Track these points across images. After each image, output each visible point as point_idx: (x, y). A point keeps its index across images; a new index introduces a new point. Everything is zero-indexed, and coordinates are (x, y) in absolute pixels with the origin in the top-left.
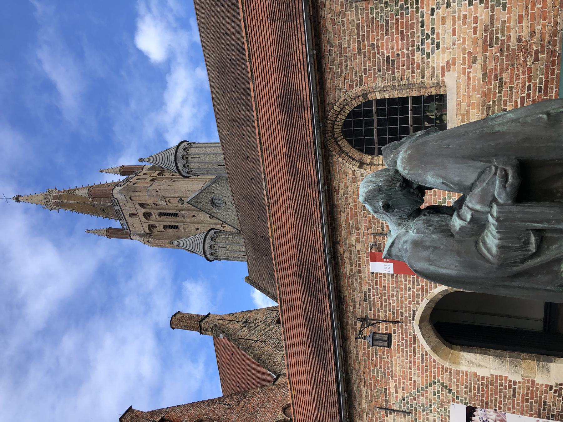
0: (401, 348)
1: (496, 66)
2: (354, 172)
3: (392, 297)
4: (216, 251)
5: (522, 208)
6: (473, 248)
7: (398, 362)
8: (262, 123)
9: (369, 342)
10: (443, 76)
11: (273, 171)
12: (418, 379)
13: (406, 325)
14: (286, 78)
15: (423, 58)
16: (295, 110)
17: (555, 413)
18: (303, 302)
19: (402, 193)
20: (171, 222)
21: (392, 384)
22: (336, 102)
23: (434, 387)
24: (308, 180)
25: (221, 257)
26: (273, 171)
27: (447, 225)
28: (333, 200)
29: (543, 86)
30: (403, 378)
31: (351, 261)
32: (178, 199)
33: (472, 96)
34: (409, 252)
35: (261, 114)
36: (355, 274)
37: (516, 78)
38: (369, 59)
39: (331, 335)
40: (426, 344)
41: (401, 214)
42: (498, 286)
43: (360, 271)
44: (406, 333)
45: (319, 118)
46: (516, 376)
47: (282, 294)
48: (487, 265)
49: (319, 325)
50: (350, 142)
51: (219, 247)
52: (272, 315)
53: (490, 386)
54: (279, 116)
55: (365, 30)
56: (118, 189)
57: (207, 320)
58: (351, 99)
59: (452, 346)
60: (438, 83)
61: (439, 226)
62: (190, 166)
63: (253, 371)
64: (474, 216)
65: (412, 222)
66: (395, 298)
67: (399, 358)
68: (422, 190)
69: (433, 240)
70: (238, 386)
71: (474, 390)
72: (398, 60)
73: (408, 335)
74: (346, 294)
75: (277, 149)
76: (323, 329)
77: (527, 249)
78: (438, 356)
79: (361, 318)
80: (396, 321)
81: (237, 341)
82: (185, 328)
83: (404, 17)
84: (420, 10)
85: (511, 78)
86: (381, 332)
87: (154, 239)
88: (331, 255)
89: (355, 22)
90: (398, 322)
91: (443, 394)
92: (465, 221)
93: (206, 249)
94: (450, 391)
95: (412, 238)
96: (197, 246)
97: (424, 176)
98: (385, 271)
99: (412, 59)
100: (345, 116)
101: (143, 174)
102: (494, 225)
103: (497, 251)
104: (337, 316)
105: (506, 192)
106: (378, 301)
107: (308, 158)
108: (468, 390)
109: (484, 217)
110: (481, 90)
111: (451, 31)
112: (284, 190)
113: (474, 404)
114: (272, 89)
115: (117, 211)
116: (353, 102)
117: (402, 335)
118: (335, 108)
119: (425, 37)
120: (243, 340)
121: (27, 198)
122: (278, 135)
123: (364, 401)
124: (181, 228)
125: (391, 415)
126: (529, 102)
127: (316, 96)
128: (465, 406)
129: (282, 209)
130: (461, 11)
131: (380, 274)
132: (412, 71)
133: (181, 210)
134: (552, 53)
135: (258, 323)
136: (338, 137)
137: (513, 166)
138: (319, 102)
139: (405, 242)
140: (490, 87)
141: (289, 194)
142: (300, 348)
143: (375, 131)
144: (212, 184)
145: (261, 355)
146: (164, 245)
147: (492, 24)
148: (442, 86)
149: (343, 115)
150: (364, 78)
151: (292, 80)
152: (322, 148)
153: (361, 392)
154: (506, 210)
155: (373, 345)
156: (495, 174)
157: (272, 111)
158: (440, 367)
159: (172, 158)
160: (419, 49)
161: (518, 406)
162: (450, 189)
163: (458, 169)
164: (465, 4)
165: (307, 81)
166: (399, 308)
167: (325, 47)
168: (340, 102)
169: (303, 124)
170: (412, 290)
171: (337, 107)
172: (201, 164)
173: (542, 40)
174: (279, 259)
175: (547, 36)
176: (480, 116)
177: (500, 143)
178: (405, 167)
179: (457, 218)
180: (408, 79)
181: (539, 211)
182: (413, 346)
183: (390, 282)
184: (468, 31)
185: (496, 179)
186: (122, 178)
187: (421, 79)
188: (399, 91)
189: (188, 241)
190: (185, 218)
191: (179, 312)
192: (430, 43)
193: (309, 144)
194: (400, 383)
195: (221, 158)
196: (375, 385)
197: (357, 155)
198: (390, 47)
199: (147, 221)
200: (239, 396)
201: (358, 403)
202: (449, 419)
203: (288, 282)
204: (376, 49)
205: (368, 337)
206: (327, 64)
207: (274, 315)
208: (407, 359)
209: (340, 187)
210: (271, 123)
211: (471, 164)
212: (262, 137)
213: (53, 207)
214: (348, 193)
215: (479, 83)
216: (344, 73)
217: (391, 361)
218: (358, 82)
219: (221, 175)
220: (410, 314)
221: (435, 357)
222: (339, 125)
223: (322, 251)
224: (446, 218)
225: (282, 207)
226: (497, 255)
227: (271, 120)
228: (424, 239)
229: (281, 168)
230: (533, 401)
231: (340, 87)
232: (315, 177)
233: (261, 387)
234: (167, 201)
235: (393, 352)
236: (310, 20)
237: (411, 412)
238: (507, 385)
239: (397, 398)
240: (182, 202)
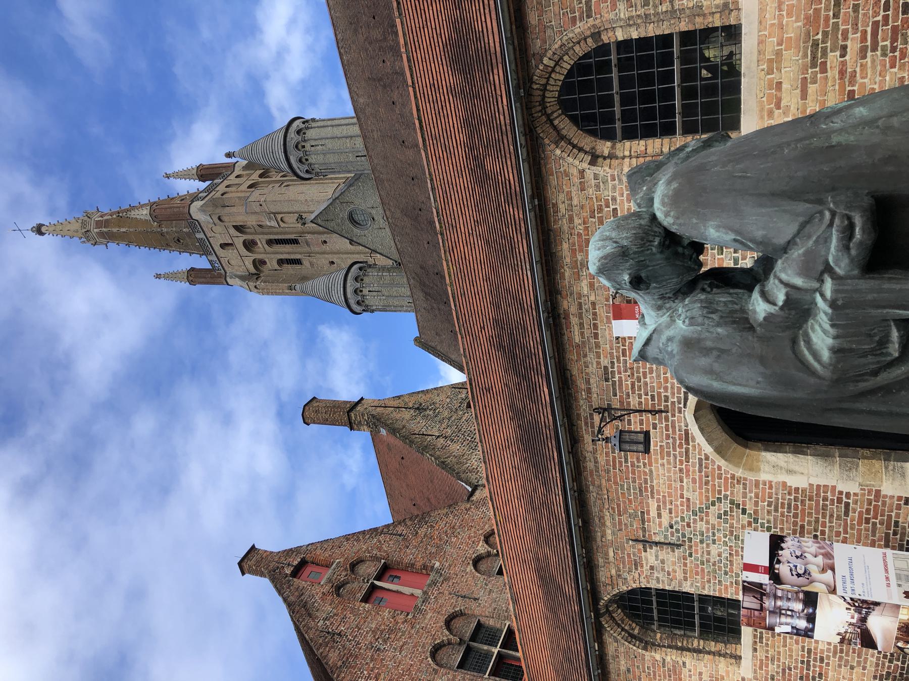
0: (666, 450)
2: (582, 172)
3: (650, 373)
4: (365, 297)
5: (877, 282)
6: (789, 352)
7: (661, 471)
8: (422, 92)
9: (615, 445)
11: (444, 174)
12: (695, 497)
13: (673, 416)
14: (458, 11)
16: (476, 67)
19: (662, 256)
20: (288, 253)
22: (546, 50)
23: (719, 506)
24: (505, 190)
25: (374, 308)
26: (444, 174)
27: (743, 311)
28: (548, 222)
30: (670, 495)
31: (582, 321)
32: (297, 215)
33: (787, 25)
35: (419, 75)
36: (589, 341)
39: (553, 435)
41: (662, 291)
42: (830, 410)
43: (596, 336)
44: (673, 427)
45: (519, 80)
46: (850, 486)
47: (472, 372)
48: (812, 380)
50: (574, 120)
51: (369, 291)
52: (459, 396)
53: (807, 502)
54: (449, 78)
56: (198, 204)
57: (359, 408)
58: (572, 44)
59: (747, 444)
61: (728, 313)
62: (310, 161)
63: (435, 481)
64: (790, 297)
65: (681, 305)
66: (654, 375)
67: (663, 465)
69: (719, 338)
70: (414, 505)
71: (783, 507)
73: (677, 430)
74: (575, 372)
75: (449, 137)
77: (884, 351)
78: (726, 460)
79: (601, 408)
80: (657, 409)
81: (408, 438)
82: (325, 422)
86: (633, 428)
87: (265, 282)
88: (548, 313)
90: (661, 411)
92: (774, 304)
93: (349, 295)
94: (744, 511)
95: (682, 333)
96: (333, 292)
97: (702, 227)
100: (563, 75)
101: (236, 177)
103: (831, 358)
104: (562, 406)
106: (627, 381)
107: (503, 152)
108: (773, 508)
109: (807, 297)
110: (803, 13)
112: (466, 206)
114: (434, 31)
115: (200, 240)
116: (577, 48)
117: (667, 430)
118: (546, 61)
120: (417, 436)
121: (53, 228)
122: (449, 113)
123: (609, 532)
124: (306, 263)
125: (652, 549)
126: (886, 31)
127: (510, 42)
129: (464, 238)
133: (303, 233)
135: (439, 409)
136: (553, 113)
138: (518, 53)
139: (670, 339)
140: (819, 6)
141: (474, 213)
142: (505, 453)
143: (617, 98)
144: (348, 188)
145: (446, 458)
146: (281, 291)
148: (732, 10)
149: (560, 73)
150: (593, 4)
151: (468, 14)
152: (525, 135)
153: (603, 517)
154: (849, 288)
156: (831, 225)
157: (438, 70)
158: (729, 476)
159: (279, 148)
161: (852, 529)
165: (494, 16)
166: (662, 390)
168: (553, 50)
169: (492, 93)
171: (550, 59)
172: (328, 156)
174: (464, 320)
176: (800, 61)
177: (840, 167)
178: (669, 212)
182: (684, 446)
185: (832, 234)
186: (203, 185)
188: (656, 25)
189: (319, 283)
190: (311, 246)
191: (314, 398)
193: (504, 128)
194: (664, 503)
195: (359, 143)
196: (625, 507)
197: (587, 141)
199: (250, 254)
200: (416, 522)
201: (599, 534)
202: (742, 552)
203: (481, 355)
205: (613, 438)
207: (463, 396)
209: (560, 198)
210: (437, 91)
212: (423, 116)
213: (98, 240)
214: (574, 208)
217: (651, 471)
218: (583, 12)
219: (363, 172)
221: (721, 462)
222: (553, 91)
223: (533, 306)
224: (740, 296)
225: (463, 235)
226: (830, 365)
227: (436, 86)
228: (703, 336)
229: (459, 168)
230: (877, 521)
231: (553, 23)
232: (517, 184)
233: (450, 506)
234: (279, 219)
235: (653, 457)
237: (683, 544)
238: (835, 498)
239: (660, 525)
240: (304, 221)
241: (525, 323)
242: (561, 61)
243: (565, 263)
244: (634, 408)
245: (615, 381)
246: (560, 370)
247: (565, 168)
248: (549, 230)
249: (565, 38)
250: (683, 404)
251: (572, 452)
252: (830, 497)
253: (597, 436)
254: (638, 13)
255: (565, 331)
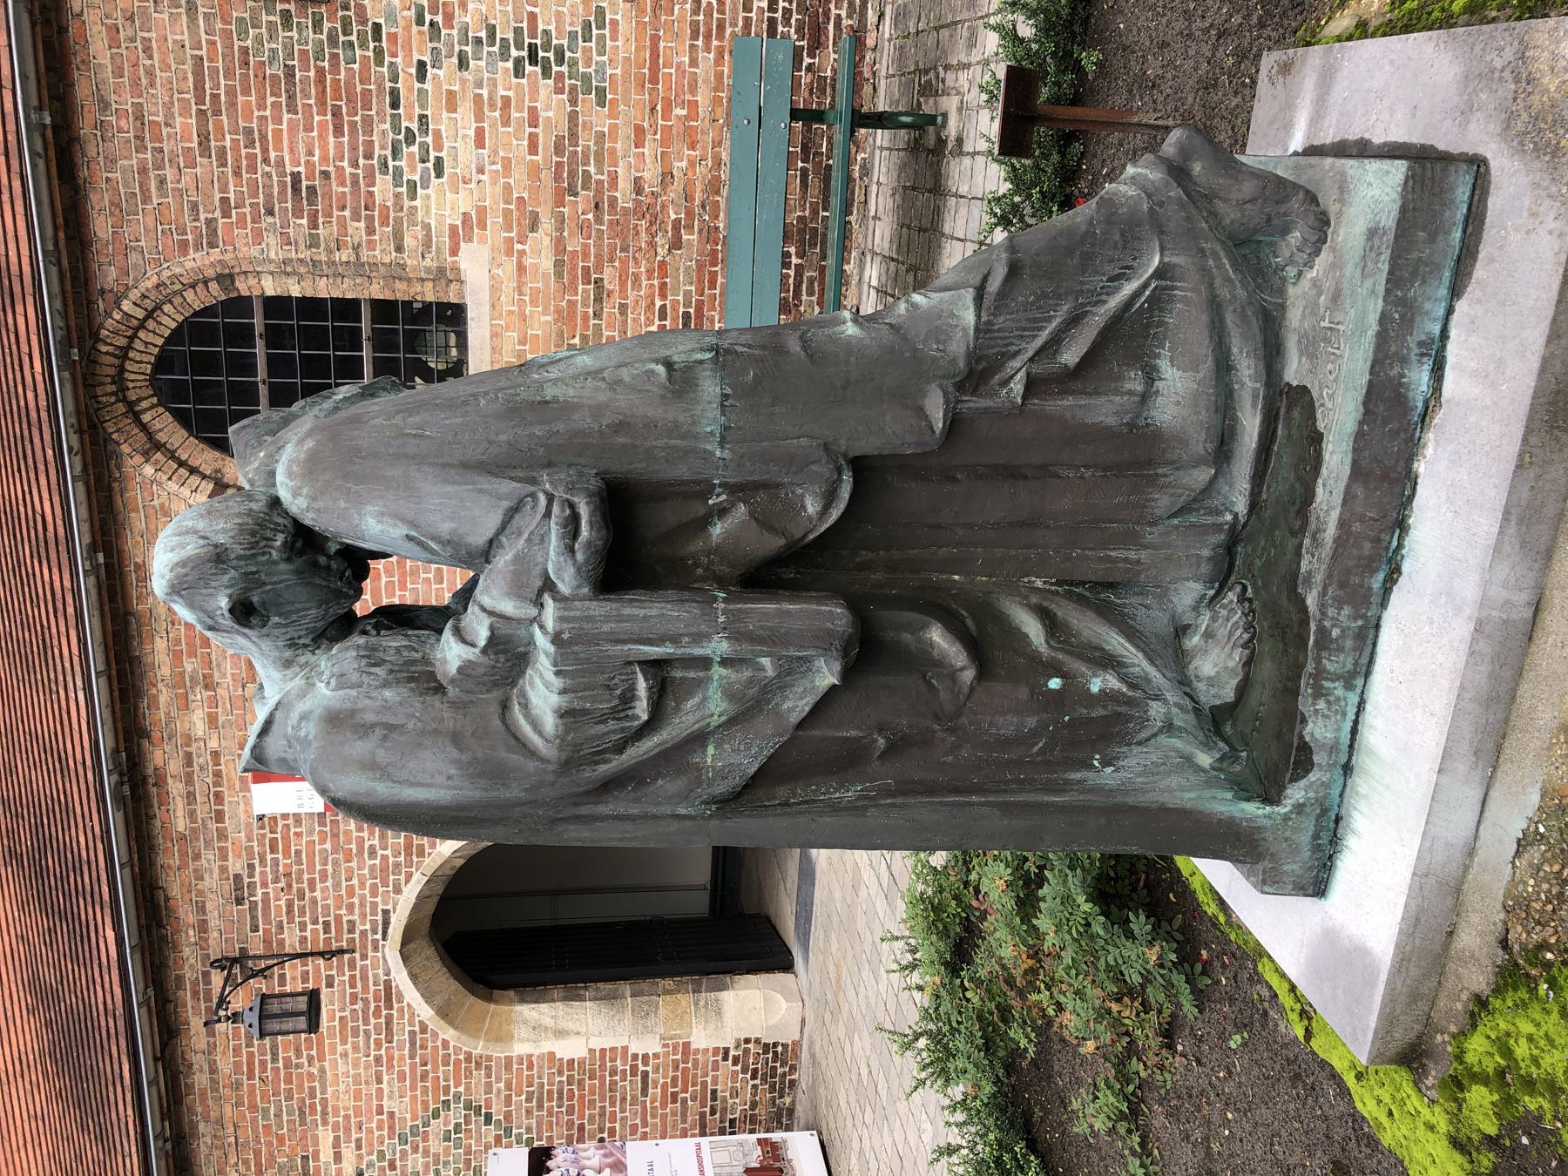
0: (350, 1024)
1: (586, 246)
5: (614, 606)
6: (497, 722)
9: (250, 1026)
10: (454, 251)
12: (400, 1106)
13: (364, 957)
15: (398, 196)
17: (737, 1115)
18: (22, 938)
21: (326, 1138)
22: (127, 288)
23: (447, 1116)
27: (426, 661)
28: (125, 598)
29: (692, 311)
31: (191, 789)
34: (315, 745)
36: (205, 827)
37: (633, 283)
38: (237, 174)
39: (121, 1029)
40: (421, 1000)
43: (220, 817)
44: (364, 978)
46: (647, 1045)
48: (532, 765)
49: (80, 1002)
50: (182, 418)
55: (222, 82)
60: (441, 271)
66: (329, 884)
67: (345, 1055)
68: (357, 562)
69: (387, 707)
71: (550, 1099)
72: (327, 188)
73: (371, 983)
74: (175, 891)
76: (95, 1014)
78: (456, 1028)
79: (227, 959)
83: (342, 70)
84: (387, 59)
85: (623, 283)
86: (288, 989)
88: (121, 775)
89: (189, 52)
90: (341, 952)
91: (471, 1131)
92: (473, 645)
94: (488, 1119)
98: (301, 806)
99: (369, 192)
102: (547, 654)
105: (574, 565)
109: (522, 632)
111: (472, 133)
113: (550, 1138)
117: (353, 986)
118: (126, 305)
119: (401, 137)
128: (527, 1150)
130: (495, 85)
131: (285, 816)
132: (367, 227)
134: (710, 233)
136: (140, 400)
137: (590, 495)
139: (304, 717)
143: (263, 391)
147: (573, 135)
149: (154, 332)
152: (80, 432)
155: (262, 1035)
156: (548, 514)
158: (462, 1057)
160: (387, 167)
161: (654, 1116)
162: (433, 557)
163: (450, 499)
164: (507, 70)
165: (20, 208)
167: (86, 109)
169: (10, 348)
170: (381, 852)
171: (134, 303)
173: (688, 197)
175: (698, 190)
178: (300, 488)
179: (452, 639)
180: (356, 248)
181: (654, 612)
182: (384, 1012)
183: (316, 838)
184: (515, 142)
187: (394, 254)
188: (331, 280)
192: (417, 157)
193: (33, 414)
194: (347, 1129)
198: (302, 149)
204: (257, 144)
205: (247, 1012)
206: (92, 165)
208: (368, 1056)
211: (485, 487)
215: (547, 285)
216: (155, 201)
217: (322, 1071)
218: (201, 236)
220: (374, 923)
221: (448, 1033)
222: (141, 362)
223: (89, 763)
226: (557, 736)
228: (360, 706)
230: (688, 1095)
231: (143, 243)
232: (59, 522)
235: (327, 1041)
236: (31, 13)
241: (70, 799)
242: (158, 312)
243: (159, 678)
244: (292, 952)
245: (256, 902)
246: (143, 890)
247: (161, 500)
248: (128, 614)
249: (166, 274)
250: (380, 932)
251: (162, 1058)
252: (620, 1068)
253: (216, 1013)
254: (302, 256)
255: (157, 811)
